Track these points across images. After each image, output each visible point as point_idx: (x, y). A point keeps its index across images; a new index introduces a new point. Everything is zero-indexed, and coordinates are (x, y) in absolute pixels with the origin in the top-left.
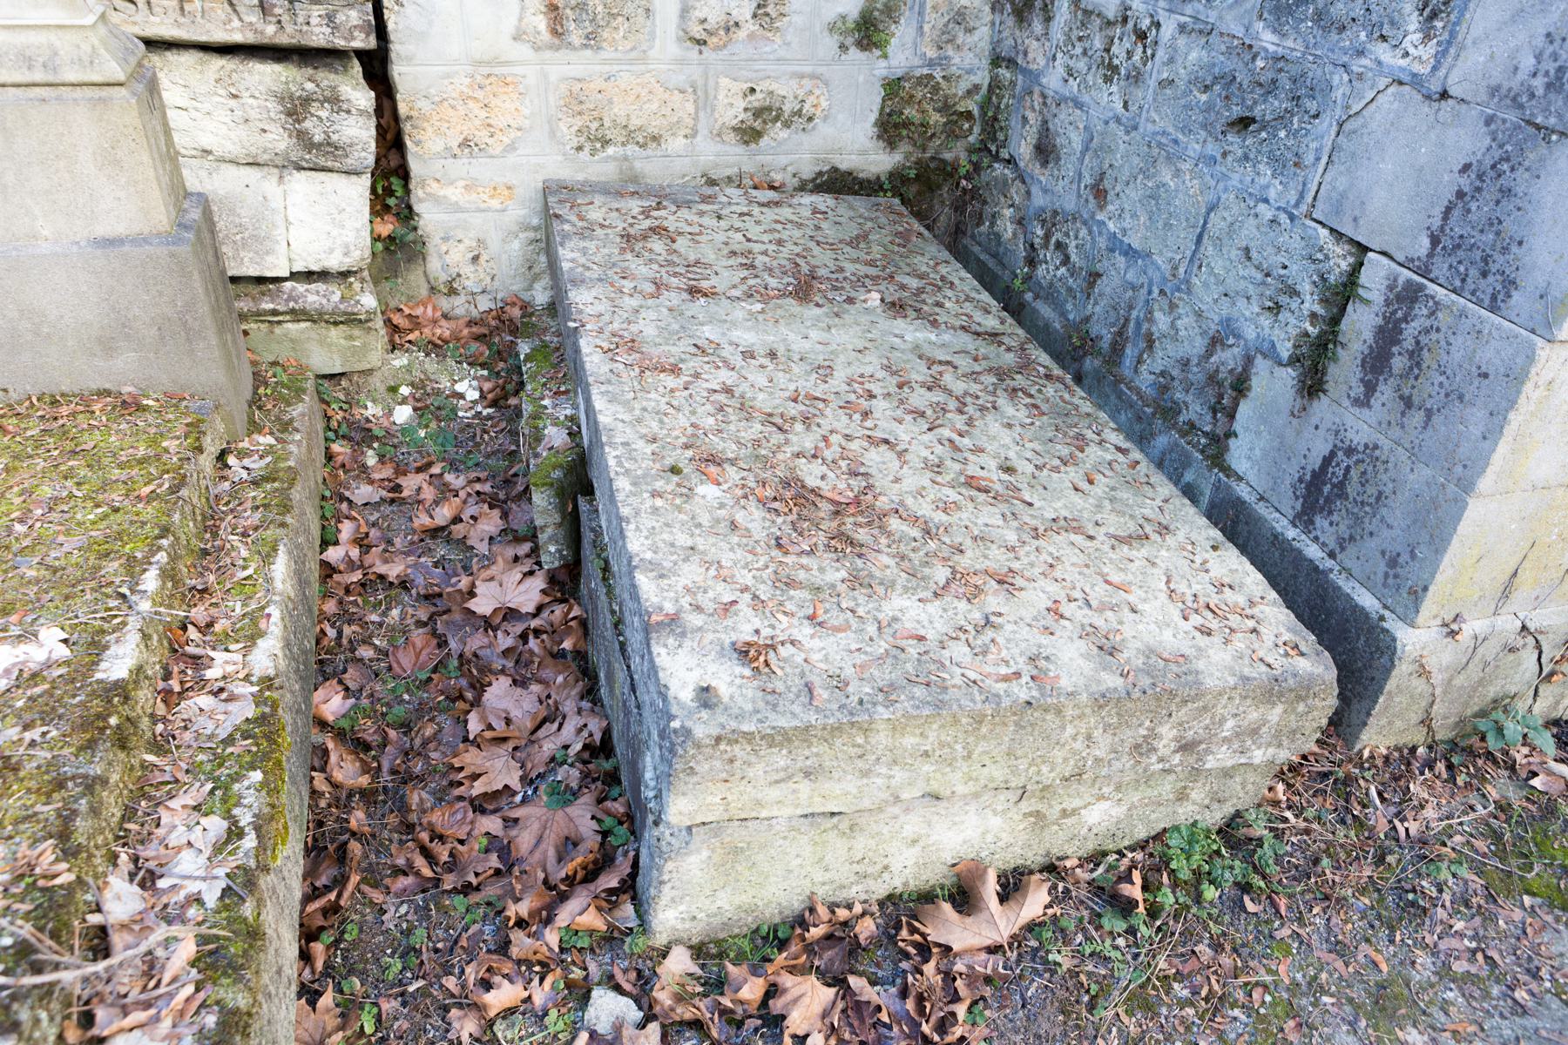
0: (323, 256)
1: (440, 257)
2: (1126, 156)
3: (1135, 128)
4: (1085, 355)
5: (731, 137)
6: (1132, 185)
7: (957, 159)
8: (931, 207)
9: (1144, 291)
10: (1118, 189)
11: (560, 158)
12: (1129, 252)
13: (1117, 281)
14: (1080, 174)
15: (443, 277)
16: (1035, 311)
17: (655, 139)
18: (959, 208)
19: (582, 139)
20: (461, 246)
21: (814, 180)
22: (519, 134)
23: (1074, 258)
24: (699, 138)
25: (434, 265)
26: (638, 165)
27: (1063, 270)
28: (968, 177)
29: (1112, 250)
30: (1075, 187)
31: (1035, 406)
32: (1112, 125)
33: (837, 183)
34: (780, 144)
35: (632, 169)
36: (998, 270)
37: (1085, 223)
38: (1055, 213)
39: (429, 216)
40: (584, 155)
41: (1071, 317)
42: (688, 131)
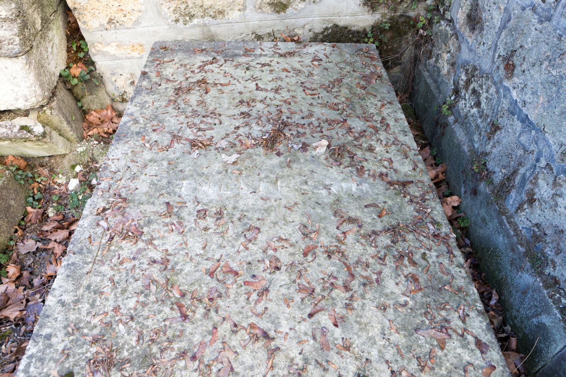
0: (13, 102)
1: (113, 84)
2: (536, 42)
3: (549, 19)
4: (481, 179)
5: (268, 9)
6: (537, 68)
7: (419, 15)
8: (400, 46)
9: (532, 157)
10: (524, 67)
11: (167, 27)
12: (525, 120)
13: (512, 138)
14: (496, 46)
15: (117, 94)
16: (453, 132)
17: (221, 12)
18: (417, 46)
19: (177, 15)
20: (122, 77)
21: (322, 33)
22: (140, 14)
23: (483, 105)
24: (248, 11)
25: (110, 88)
26: (213, 29)
27: (475, 110)
28: (424, 28)
29: (513, 114)
30: (491, 53)
31: (415, 279)
32: (528, 12)
33: (337, 35)
34: (300, 11)
35: (209, 31)
36: (435, 92)
37: (495, 83)
38: (475, 69)
39: (102, 65)
40: (180, 24)
41: (476, 146)
42: (241, 7)
